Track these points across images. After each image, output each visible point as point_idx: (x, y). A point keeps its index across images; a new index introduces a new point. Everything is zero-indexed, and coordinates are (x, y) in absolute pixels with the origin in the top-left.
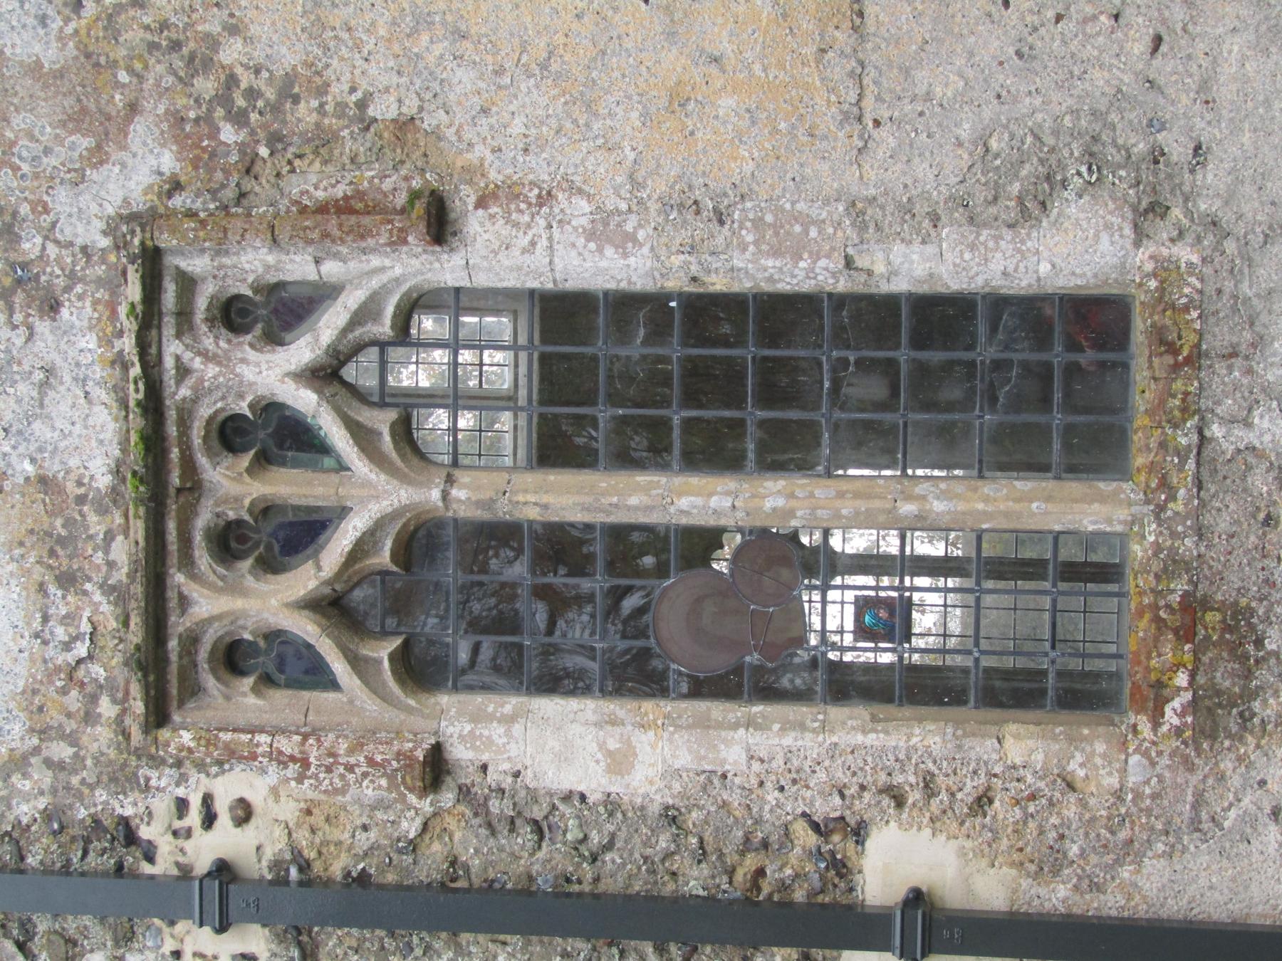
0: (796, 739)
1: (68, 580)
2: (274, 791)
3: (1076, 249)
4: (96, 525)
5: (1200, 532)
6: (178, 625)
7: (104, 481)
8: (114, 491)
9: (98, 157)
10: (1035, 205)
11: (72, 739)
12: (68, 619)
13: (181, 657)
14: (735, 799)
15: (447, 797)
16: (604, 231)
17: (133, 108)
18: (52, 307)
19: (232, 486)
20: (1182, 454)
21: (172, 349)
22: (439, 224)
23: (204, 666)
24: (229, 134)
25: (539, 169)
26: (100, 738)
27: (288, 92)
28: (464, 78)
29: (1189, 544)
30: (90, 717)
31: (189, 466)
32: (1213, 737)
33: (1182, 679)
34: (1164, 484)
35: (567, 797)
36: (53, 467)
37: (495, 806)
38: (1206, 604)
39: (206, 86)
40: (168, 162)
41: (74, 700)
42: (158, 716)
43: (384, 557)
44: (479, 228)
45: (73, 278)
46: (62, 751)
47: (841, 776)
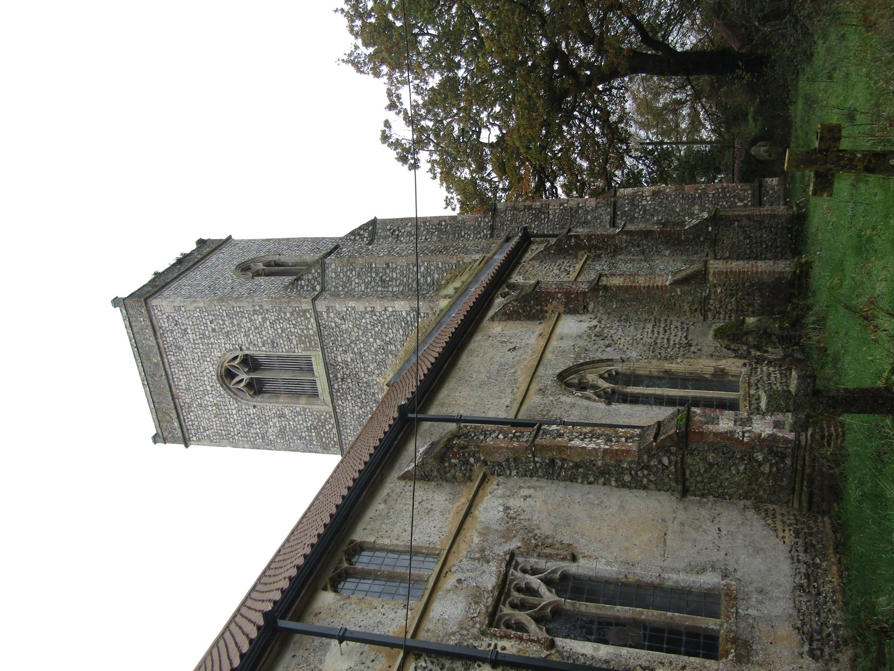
0: (642, 613)
1: (476, 603)
2: (512, 646)
3: (710, 579)
4: (486, 595)
5: (737, 627)
6: (499, 614)
7: (490, 588)
8: (492, 591)
9: (506, 542)
10: (703, 570)
11: (468, 630)
12: (475, 609)
13: (671, 31)
14: (623, 660)
15: (553, 651)
16: (608, 563)
17: (515, 536)
18: (488, 562)
19: (517, 596)
20: (733, 613)
21: (512, 570)
22: (574, 559)
23: (512, 590)
24: (533, 541)
25: (596, 554)
26: (475, 631)
27: (547, 537)
28: (583, 541)
29: (734, 628)
30: (473, 627)
31: (509, 590)
32: (740, 662)
33: (733, 651)
34: (728, 617)
35: (583, 655)
36: (480, 585)
37: (565, 654)
38: (738, 639)
39: (530, 535)
40: (519, 545)
41: (471, 623)
42: (490, 625)
43: (558, 575)
44: (582, 562)
45: (494, 558)
46: (465, 632)
47: (649, 658)
